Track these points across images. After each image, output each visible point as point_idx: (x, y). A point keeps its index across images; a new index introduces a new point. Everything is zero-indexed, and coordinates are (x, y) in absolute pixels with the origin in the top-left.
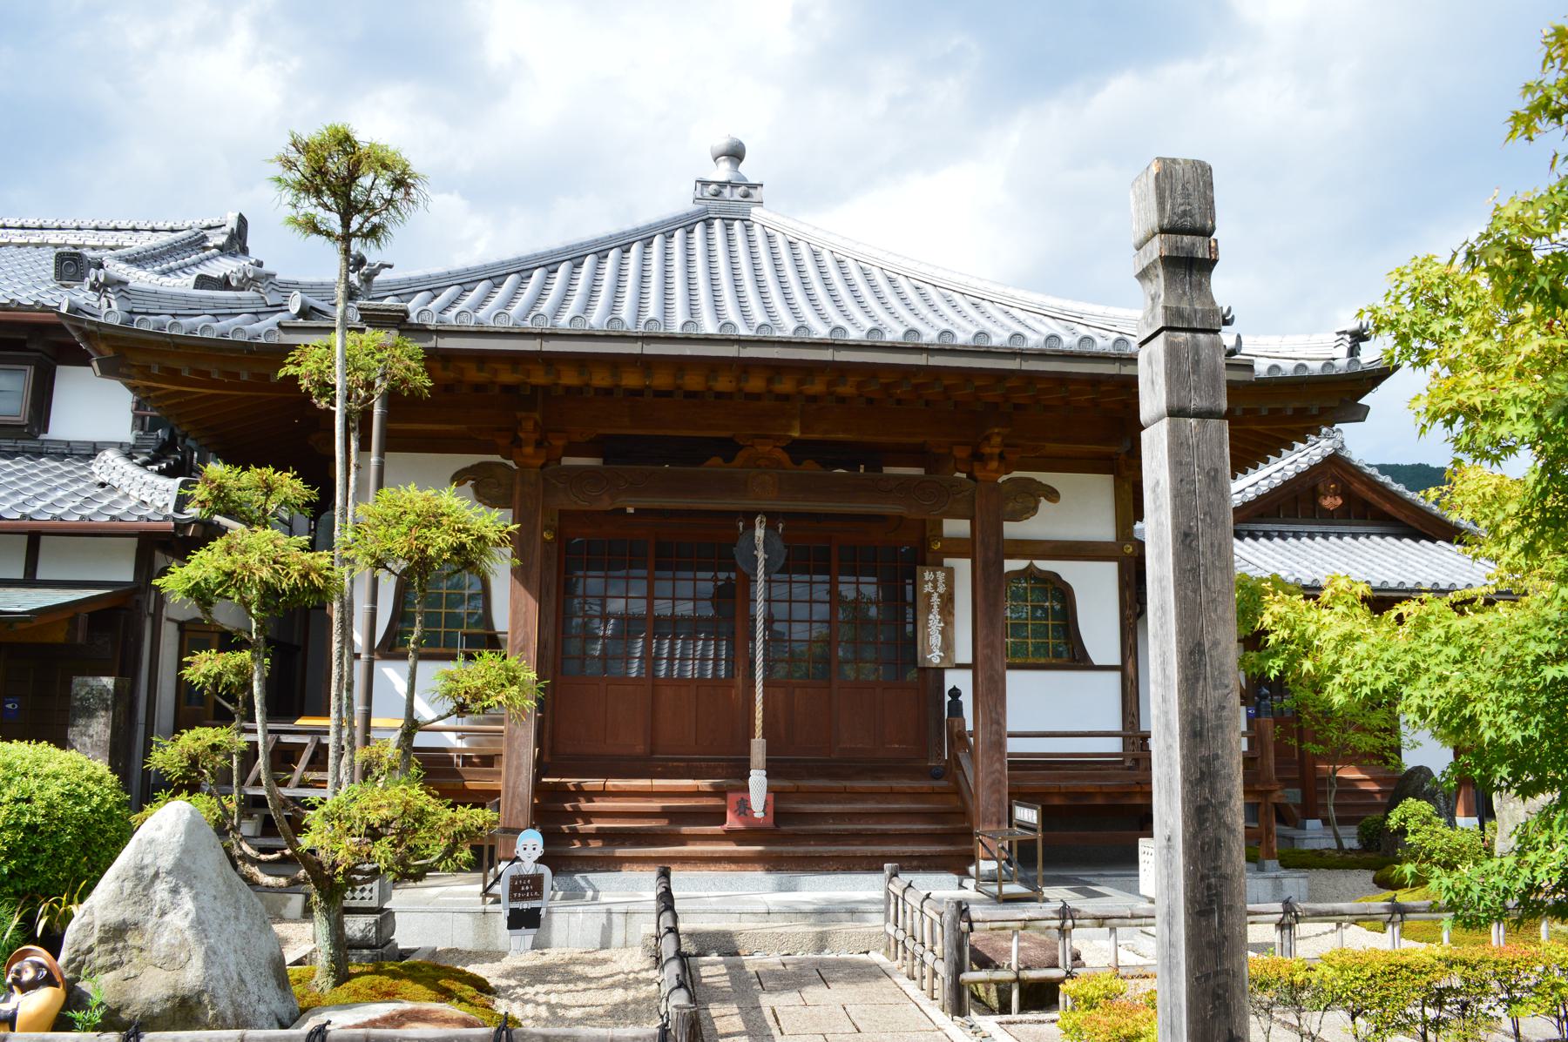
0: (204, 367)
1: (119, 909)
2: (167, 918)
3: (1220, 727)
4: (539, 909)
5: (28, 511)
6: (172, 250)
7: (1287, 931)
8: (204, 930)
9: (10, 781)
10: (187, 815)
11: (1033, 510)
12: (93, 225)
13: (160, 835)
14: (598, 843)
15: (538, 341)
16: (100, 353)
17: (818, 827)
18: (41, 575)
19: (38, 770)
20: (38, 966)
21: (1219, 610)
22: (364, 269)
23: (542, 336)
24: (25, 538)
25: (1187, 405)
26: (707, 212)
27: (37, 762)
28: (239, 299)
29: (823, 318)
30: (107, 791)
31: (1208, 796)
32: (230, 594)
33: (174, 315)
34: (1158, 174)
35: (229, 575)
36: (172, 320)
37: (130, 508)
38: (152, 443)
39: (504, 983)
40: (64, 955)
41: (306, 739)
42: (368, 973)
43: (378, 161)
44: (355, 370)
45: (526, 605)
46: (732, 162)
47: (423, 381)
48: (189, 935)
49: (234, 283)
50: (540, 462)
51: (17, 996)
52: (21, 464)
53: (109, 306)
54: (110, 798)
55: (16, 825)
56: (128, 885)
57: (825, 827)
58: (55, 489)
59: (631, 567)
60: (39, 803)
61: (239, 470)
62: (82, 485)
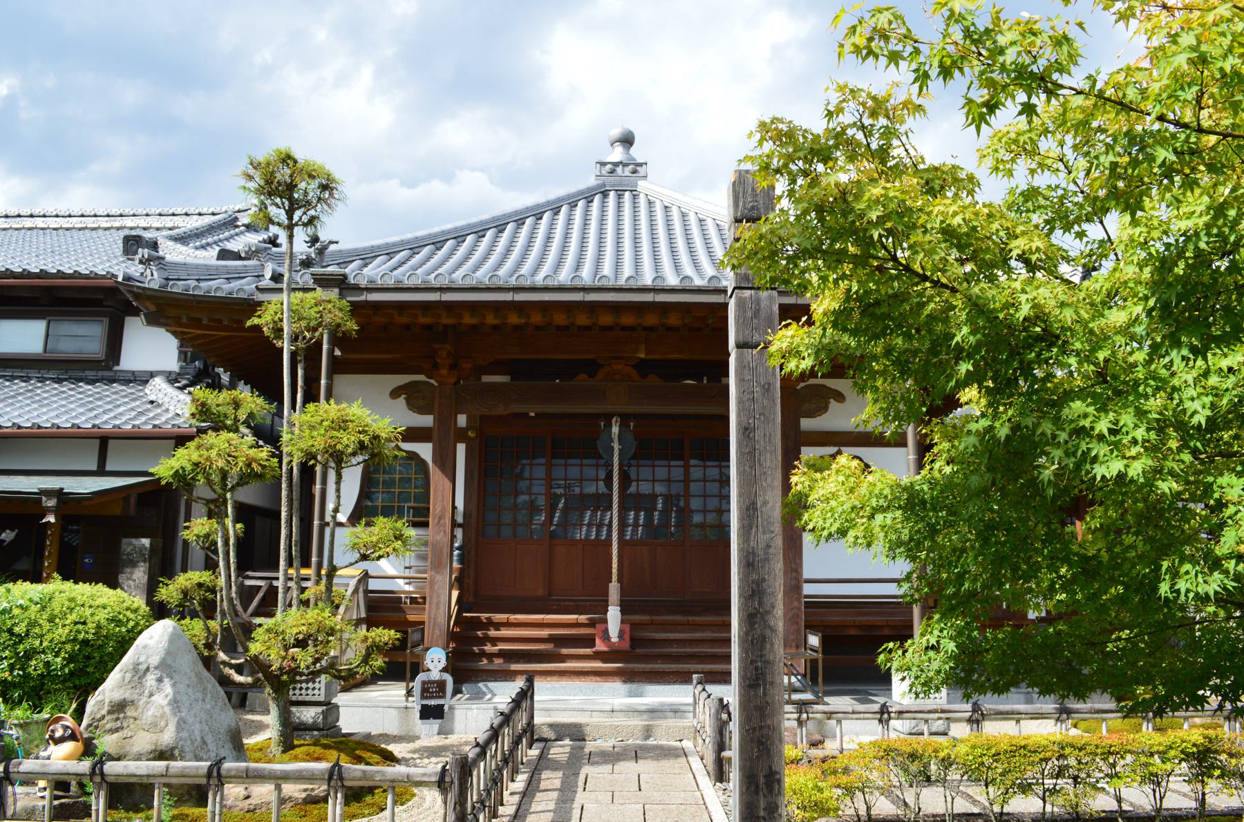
0: (218, 317)
1: (122, 692)
2: (153, 698)
3: (767, 560)
4: (443, 705)
5: (97, 422)
6: (211, 229)
7: (975, 726)
8: (178, 707)
9: (72, 610)
10: (171, 629)
11: (825, 409)
12: (157, 212)
13: (151, 642)
14: (500, 661)
15: (439, 293)
16: (147, 308)
17: (665, 650)
18: (109, 468)
19: (93, 603)
20: (66, 728)
21: (769, 480)
22: (318, 245)
23: (441, 290)
24: (98, 441)
25: (750, 340)
26: (604, 185)
27: (92, 597)
28: (245, 266)
29: (677, 267)
30: (140, 618)
31: (757, 606)
32: (199, 478)
33: (198, 280)
34: (734, 182)
35: (197, 465)
36: (195, 283)
37: (168, 419)
38: (191, 371)
39: (408, 756)
40: (85, 722)
41: (259, 583)
42: (308, 745)
43: (307, 173)
44: (299, 319)
45: (443, 485)
46: (624, 146)
47: (352, 326)
48: (167, 710)
49: (243, 255)
50: (454, 380)
51: (52, 748)
52: (100, 388)
53: (152, 275)
54: (142, 622)
55: (75, 640)
56: (129, 676)
57: (669, 650)
58: (119, 406)
59: (569, 458)
60: (90, 625)
61: (217, 391)
62: (138, 403)
